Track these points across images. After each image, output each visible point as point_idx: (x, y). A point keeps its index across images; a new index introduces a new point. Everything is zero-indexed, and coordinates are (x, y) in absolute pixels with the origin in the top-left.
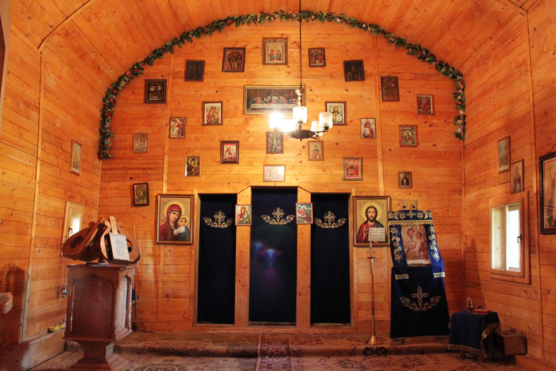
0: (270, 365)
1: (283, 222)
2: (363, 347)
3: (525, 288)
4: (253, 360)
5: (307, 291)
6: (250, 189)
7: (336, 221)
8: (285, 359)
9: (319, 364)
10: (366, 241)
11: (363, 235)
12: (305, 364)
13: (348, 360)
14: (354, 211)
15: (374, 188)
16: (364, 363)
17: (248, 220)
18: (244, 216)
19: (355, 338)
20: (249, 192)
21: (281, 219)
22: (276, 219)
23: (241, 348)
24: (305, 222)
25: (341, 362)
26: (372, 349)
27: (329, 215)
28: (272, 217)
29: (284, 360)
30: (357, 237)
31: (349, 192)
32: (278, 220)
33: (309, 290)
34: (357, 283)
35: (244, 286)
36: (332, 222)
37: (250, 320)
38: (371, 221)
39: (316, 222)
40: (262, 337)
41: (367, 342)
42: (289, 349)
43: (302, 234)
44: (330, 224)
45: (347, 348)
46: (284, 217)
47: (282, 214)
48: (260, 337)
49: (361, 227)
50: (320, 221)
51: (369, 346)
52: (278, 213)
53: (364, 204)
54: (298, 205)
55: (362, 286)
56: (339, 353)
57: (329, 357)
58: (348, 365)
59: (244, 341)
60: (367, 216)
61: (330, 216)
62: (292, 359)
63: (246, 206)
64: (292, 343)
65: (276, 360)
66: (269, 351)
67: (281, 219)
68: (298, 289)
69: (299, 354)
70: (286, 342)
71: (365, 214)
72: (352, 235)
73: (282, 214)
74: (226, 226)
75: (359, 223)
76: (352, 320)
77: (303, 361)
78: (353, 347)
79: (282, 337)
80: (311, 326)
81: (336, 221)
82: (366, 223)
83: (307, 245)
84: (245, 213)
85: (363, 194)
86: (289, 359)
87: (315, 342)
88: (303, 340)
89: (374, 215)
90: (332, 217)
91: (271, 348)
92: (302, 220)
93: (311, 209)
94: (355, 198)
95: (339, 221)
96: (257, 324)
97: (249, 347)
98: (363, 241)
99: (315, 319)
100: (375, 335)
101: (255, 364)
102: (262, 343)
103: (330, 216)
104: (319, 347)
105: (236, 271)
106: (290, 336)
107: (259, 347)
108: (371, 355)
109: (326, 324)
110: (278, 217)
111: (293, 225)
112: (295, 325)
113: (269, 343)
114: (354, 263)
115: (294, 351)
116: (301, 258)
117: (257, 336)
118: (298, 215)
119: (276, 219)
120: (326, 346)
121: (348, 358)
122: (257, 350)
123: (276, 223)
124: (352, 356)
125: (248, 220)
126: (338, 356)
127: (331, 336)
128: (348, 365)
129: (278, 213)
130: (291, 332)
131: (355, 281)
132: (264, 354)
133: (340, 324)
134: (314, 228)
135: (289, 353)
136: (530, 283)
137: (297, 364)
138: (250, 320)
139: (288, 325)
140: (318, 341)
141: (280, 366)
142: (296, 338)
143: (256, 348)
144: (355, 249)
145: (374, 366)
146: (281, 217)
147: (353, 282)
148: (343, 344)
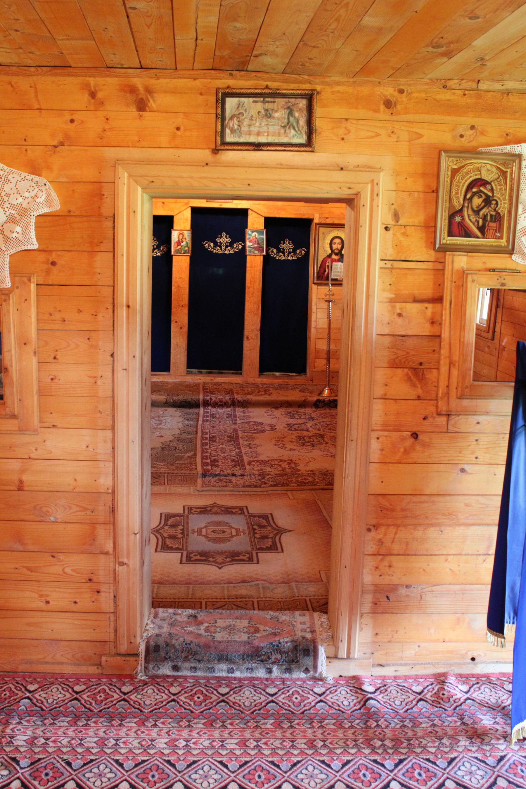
0: (213, 414)
1: (229, 251)
2: (314, 398)
3: (489, 344)
4: (195, 410)
5: (256, 335)
6: (189, 211)
7: (294, 251)
8: (229, 409)
9: (266, 415)
10: (327, 278)
11: (325, 271)
12: (250, 414)
13: (297, 412)
14: (317, 242)
15: (342, 214)
16: (313, 415)
17: (186, 248)
18: (182, 244)
19: (308, 390)
20: (188, 214)
21: (227, 247)
22: (220, 247)
23: (181, 397)
24: (256, 252)
25: (290, 413)
26: (324, 401)
27: (287, 243)
28: (216, 244)
29: (229, 410)
30: (318, 273)
31: (311, 217)
32: (223, 248)
33: (259, 334)
34: (315, 328)
35: (181, 328)
36: (290, 253)
37: (188, 368)
38: (336, 254)
39: (270, 252)
40: (204, 386)
41: (321, 393)
42: (234, 399)
43: (252, 267)
44: (286, 254)
45: (297, 399)
46: (231, 245)
47: (229, 240)
48: (201, 387)
49: (324, 261)
50: (275, 251)
51: (321, 398)
52: (224, 239)
53: (328, 233)
54: (248, 232)
55: (320, 331)
56: (288, 404)
57: (277, 408)
58: (296, 416)
59: (183, 390)
60: (331, 247)
61: (287, 245)
62: (237, 409)
63: (185, 232)
64: (237, 393)
65: (220, 410)
66: (212, 401)
67: (227, 247)
68: (246, 332)
69: (245, 404)
70: (230, 392)
71: (329, 246)
72: (313, 270)
73: (229, 240)
74: (159, 254)
75: (322, 256)
76: (308, 371)
77: (248, 412)
78: (303, 399)
79: (226, 387)
80: (260, 375)
81: (294, 251)
82: (330, 256)
83: (258, 281)
84: (184, 240)
85: (329, 221)
86: (235, 410)
87: (263, 393)
88: (250, 390)
89: (339, 247)
90: (290, 246)
91: (214, 398)
92: (253, 250)
93: (264, 237)
94: (317, 226)
95: (298, 251)
96: (196, 373)
97: (190, 397)
98: (323, 277)
99: (265, 367)
100: (329, 387)
101: (198, 414)
102: (204, 393)
103: (287, 245)
104: (267, 398)
105: (172, 310)
106: (234, 385)
107: (201, 397)
108: (323, 407)
109: (277, 374)
110: (224, 244)
111: (242, 255)
112: (241, 374)
113: (212, 393)
114: (313, 304)
115: (239, 402)
116: (251, 295)
117: (197, 385)
118: (248, 244)
119: (220, 247)
120: (275, 397)
121: (297, 409)
122: (199, 399)
123: (220, 252)
124: (302, 408)
125: (186, 248)
126: (287, 407)
127: (280, 387)
128: (296, 416)
129: (224, 239)
130: (236, 382)
131: (313, 324)
132: (206, 404)
133: (295, 374)
134: (267, 259)
135: (234, 404)
136: (493, 339)
137: (242, 414)
138: (188, 368)
139: (233, 373)
140: (266, 392)
141: (225, 416)
142: (242, 388)
143: (197, 397)
144: (314, 287)
145: (322, 418)
146: (228, 244)
147: (311, 326)
148: (294, 396)
